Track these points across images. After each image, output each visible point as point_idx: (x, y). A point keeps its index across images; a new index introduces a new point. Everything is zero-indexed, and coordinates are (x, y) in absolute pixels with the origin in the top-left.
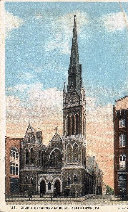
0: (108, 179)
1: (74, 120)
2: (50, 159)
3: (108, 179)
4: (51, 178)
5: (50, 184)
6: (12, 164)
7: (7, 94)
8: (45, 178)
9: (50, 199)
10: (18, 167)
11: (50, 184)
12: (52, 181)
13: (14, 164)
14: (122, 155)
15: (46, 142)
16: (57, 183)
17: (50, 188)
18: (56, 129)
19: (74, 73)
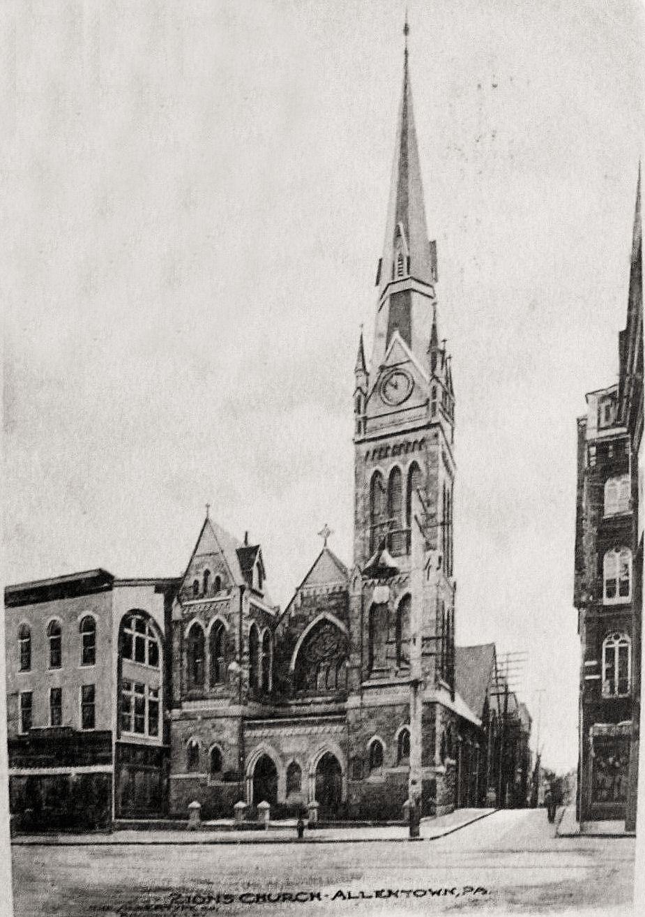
0: (557, 746)
1: (400, 490)
2: (302, 657)
3: (557, 746)
4: (299, 745)
5: (294, 769)
6: (129, 688)
7: (12, 844)
8: (276, 746)
9: (294, 834)
10: (160, 698)
11: (294, 769)
12: (304, 756)
13: (140, 689)
14: (617, 637)
15: (279, 592)
16: (328, 764)
17: (293, 786)
18: (326, 533)
19: (361, 337)
